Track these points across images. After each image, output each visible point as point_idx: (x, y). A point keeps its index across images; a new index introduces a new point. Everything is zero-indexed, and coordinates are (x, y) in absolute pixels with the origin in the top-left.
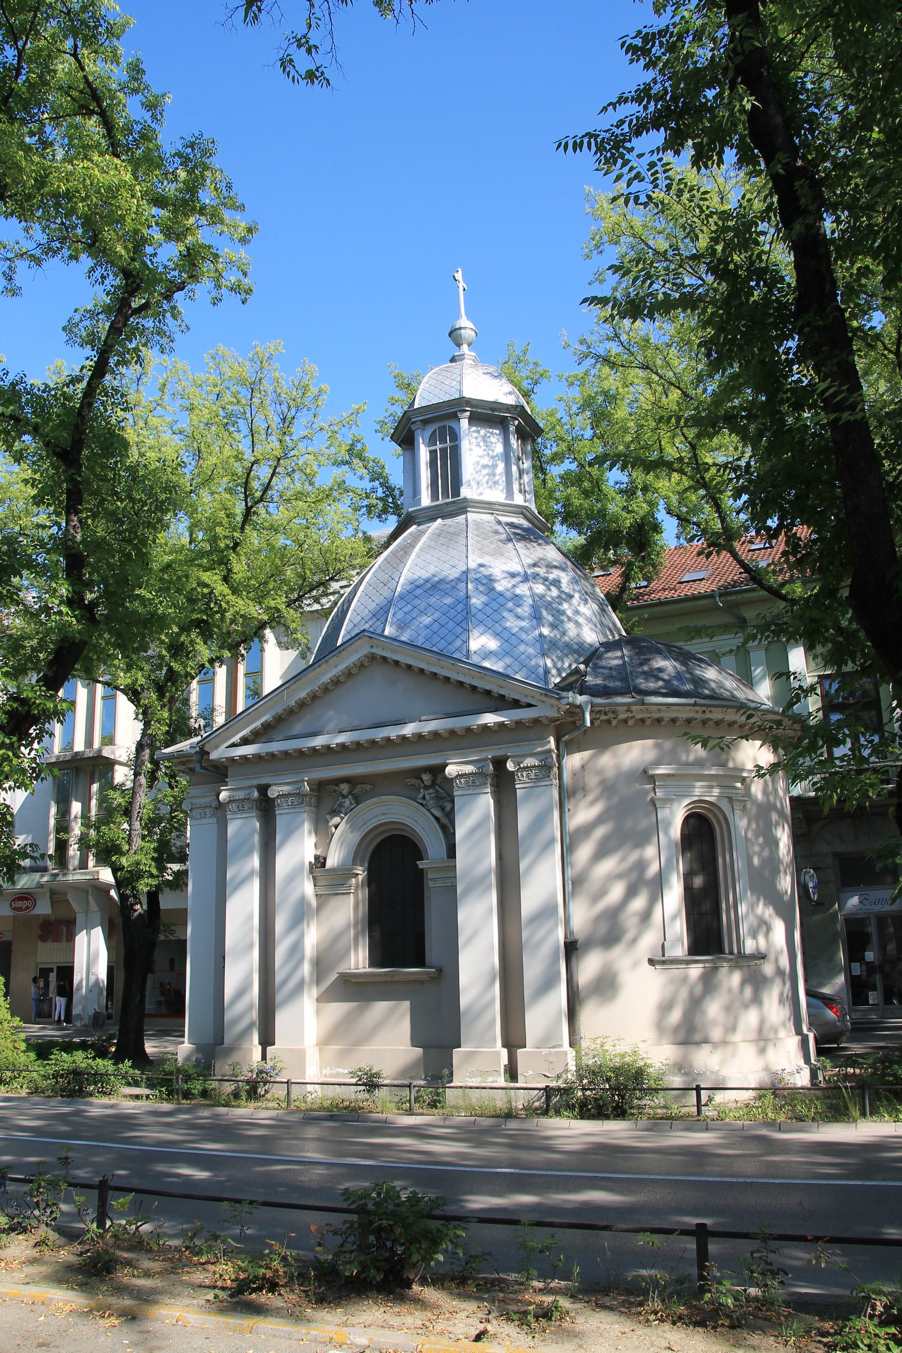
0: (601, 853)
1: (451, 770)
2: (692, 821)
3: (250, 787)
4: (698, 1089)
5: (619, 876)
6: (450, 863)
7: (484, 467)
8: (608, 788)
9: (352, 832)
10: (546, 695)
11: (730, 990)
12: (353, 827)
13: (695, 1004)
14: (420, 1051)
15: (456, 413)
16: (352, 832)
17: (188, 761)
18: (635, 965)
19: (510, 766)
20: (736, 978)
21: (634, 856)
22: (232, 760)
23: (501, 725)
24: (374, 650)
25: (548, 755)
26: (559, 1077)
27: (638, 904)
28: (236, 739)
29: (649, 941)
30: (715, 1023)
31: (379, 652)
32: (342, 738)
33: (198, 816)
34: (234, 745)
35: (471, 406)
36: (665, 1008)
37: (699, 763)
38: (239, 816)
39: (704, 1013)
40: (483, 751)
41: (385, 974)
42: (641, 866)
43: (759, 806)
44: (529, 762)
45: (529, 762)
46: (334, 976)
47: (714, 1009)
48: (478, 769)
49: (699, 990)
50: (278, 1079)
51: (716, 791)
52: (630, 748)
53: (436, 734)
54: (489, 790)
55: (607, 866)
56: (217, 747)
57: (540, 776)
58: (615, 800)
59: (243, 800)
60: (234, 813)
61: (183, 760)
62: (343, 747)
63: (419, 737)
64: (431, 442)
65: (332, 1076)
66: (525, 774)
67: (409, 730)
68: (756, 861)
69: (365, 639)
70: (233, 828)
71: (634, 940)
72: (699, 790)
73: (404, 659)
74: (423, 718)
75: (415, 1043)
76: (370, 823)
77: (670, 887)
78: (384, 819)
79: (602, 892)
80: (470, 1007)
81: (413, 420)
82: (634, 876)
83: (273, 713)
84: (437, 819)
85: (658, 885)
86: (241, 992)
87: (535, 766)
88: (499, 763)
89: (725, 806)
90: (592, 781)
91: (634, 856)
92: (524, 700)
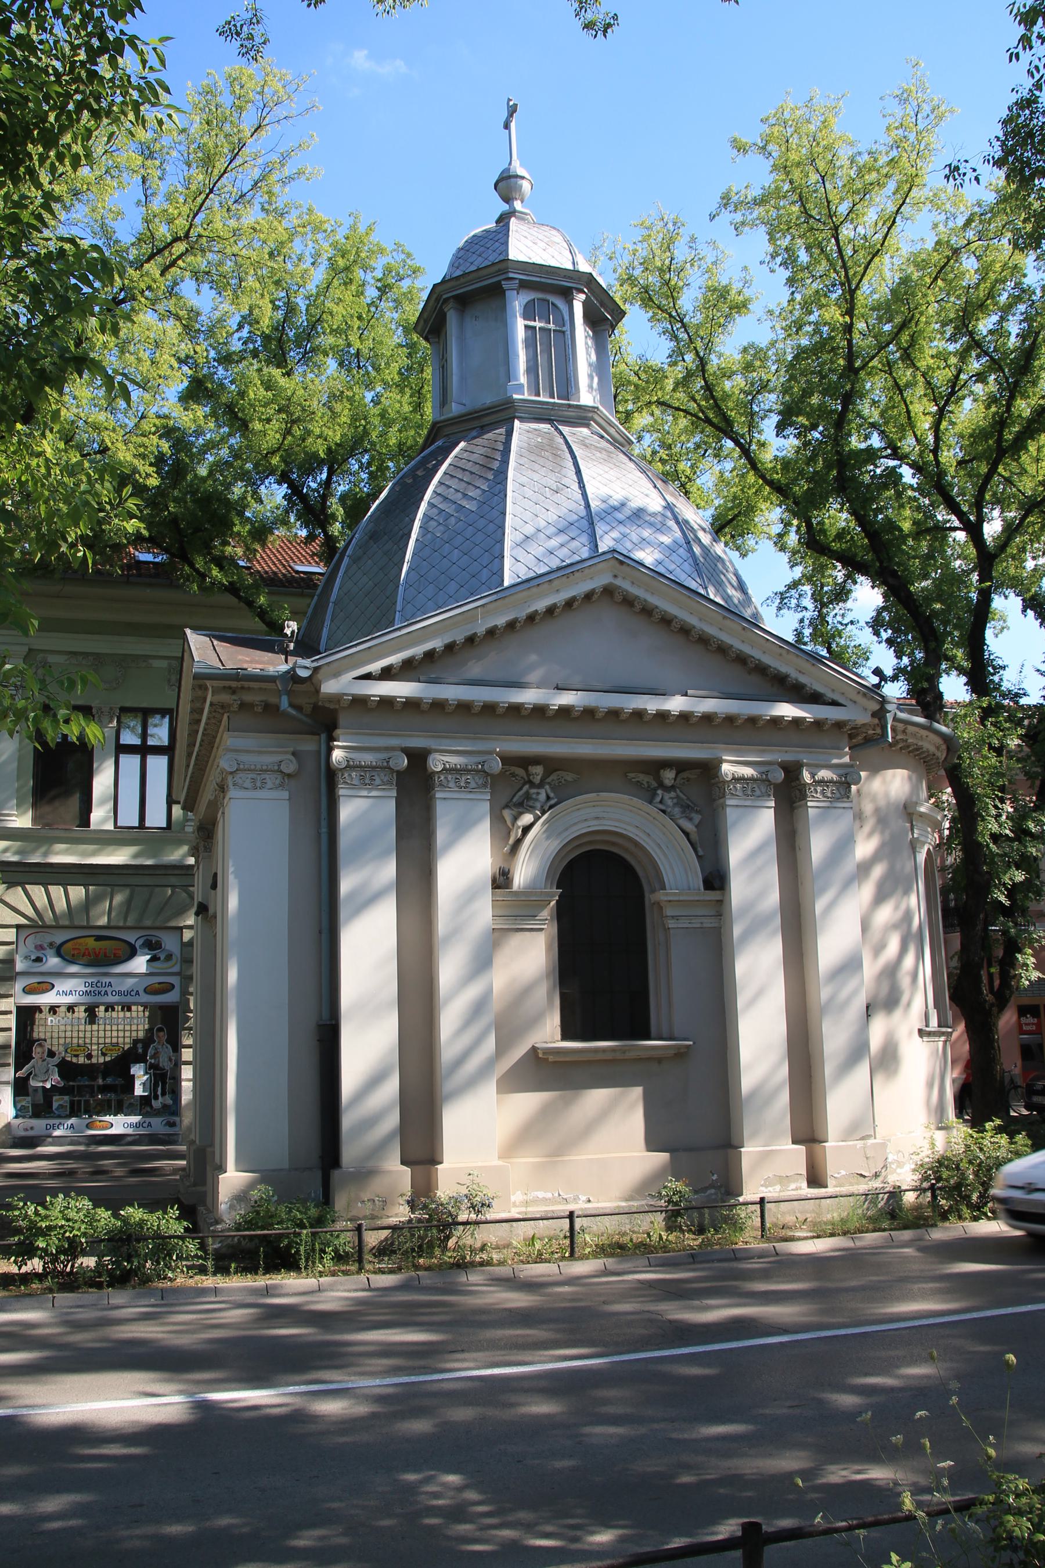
3: (392, 749)
5: (895, 926)
10: (865, 695)
12: (549, 832)
14: (664, 1156)
15: (571, 288)
16: (548, 838)
19: (807, 777)
22: (360, 702)
23: (797, 722)
24: (618, 582)
26: (876, 1175)
28: (375, 667)
31: (626, 585)
32: (567, 699)
33: (248, 784)
34: (368, 677)
38: (365, 793)
40: (764, 751)
44: (824, 774)
45: (824, 774)
48: (761, 773)
50: (490, 1216)
53: (708, 718)
54: (772, 804)
56: (337, 674)
57: (838, 795)
59: (373, 768)
60: (353, 787)
61: (234, 684)
62: (565, 711)
63: (685, 717)
65: (527, 1203)
66: (819, 789)
67: (676, 704)
69: (613, 562)
70: (349, 810)
71: (909, 1004)
74: (690, 692)
75: (653, 1143)
78: (595, 826)
81: (511, 275)
83: (448, 640)
84: (687, 834)
86: (374, 1081)
88: (792, 771)
92: (830, 695)
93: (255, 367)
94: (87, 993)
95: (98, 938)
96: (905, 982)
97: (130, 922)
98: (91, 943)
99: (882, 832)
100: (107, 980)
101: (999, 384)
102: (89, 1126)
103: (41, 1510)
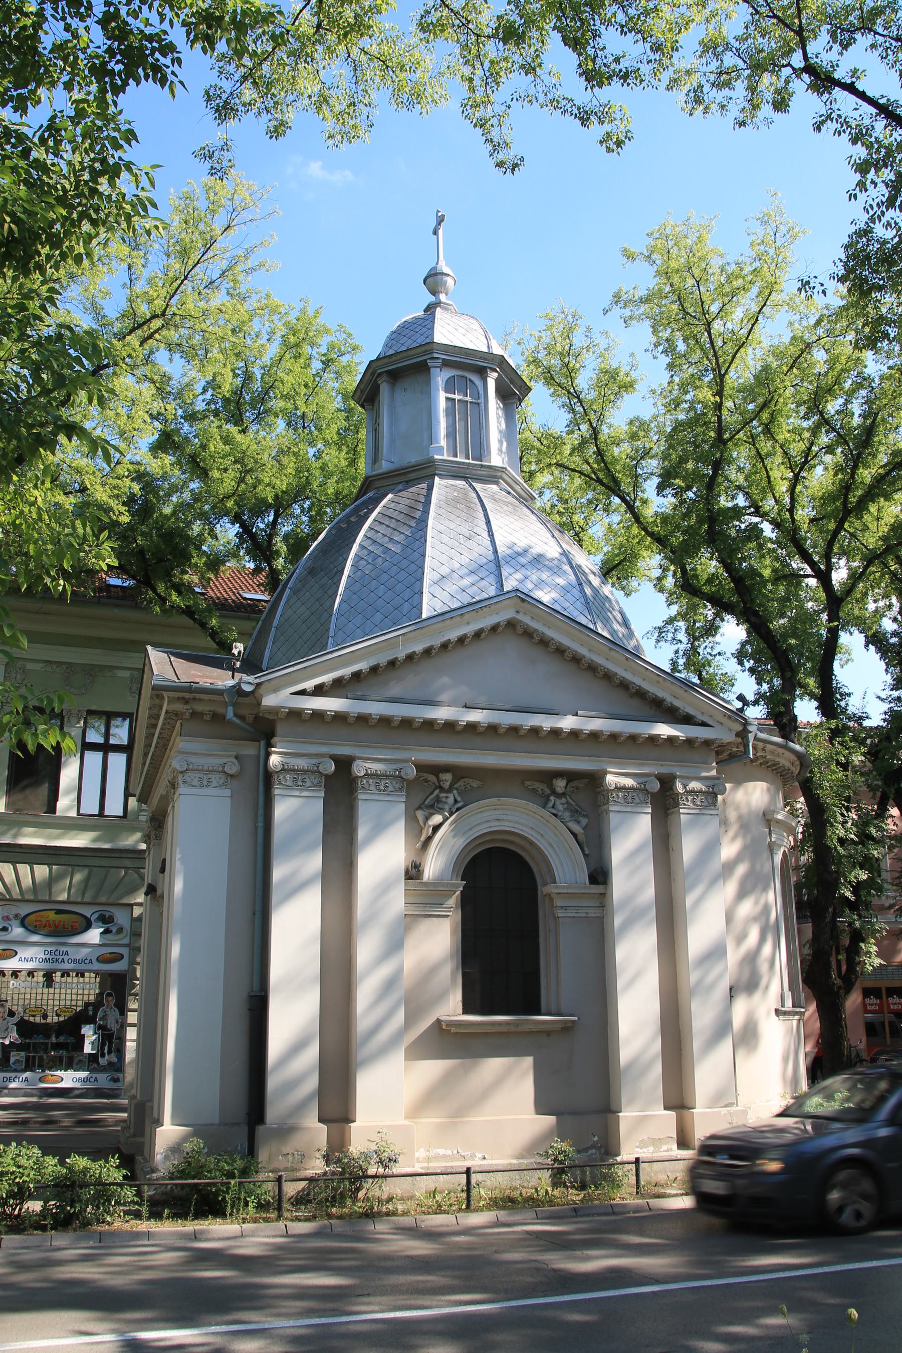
1: (611, 780)
3: (322, 755)
6: (597, 889)
9: (454, 836)
10: (730, 717)
12: (456, 830)
15: (486, 368)
16: (454, 836)
17: (194, 699)
23: (671, 740)
24: (520, 617)
25: (717, 782)
28: (309, 685)
31: (526, 620)
32: (475, 716)
34: (303, 693)
38: (297, 793)
40: (643, 764)
41: (507, 1023)
44: (694, 785)
46: (426, 1023)
48: (708, 787)
53: (595, 735)
56: (276, 690)
57: (706, 804)
59: (305, 772)
61: (187, 695)
63: (575, 734)
64: (450, 387)
65: (429, 1159)
66: (690, 798)
67: (568, 723)
73: (469, 629)
75: (541, 1108)
76: (476, 829)
80: (631, 1064)
81: (435, 355)
84: (575, 835)
87: (700, 792)
88: (667, 782)
92: (700, 717)
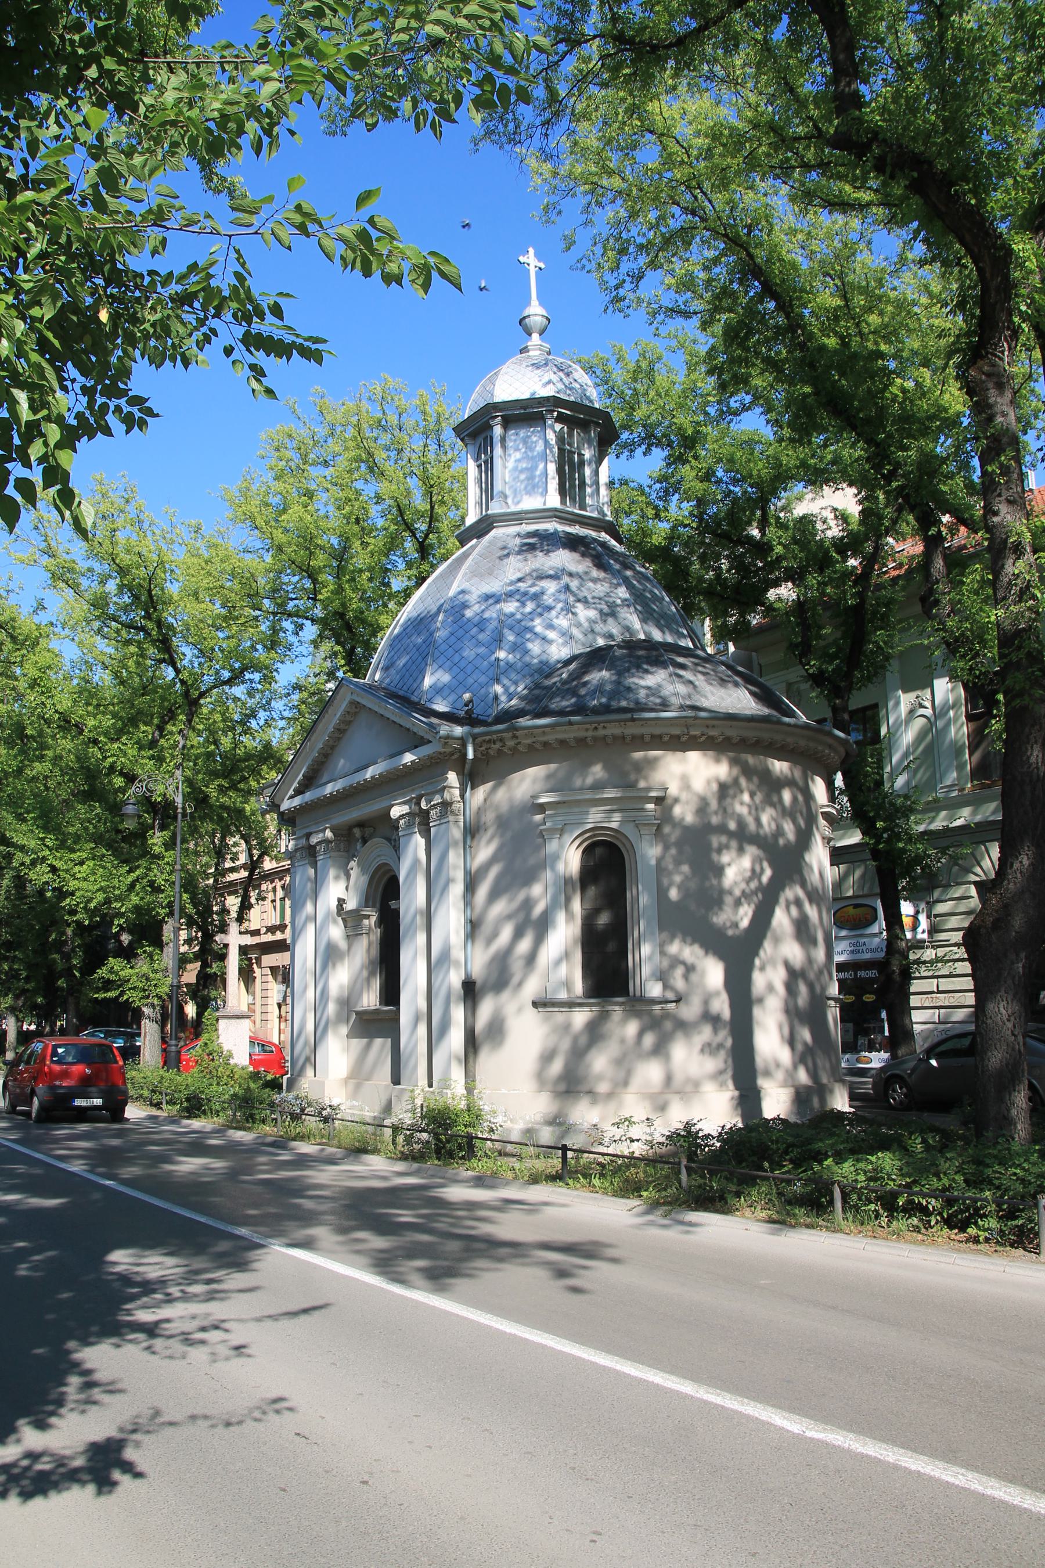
0: (494, 895)
1: (396, 812)
2: (599, 851)
4: (565, 1149)
5: (509, 917)
7: (521, 471)
8: (503, 823)
11: (623, 1041)
13: (579, 1053)
18: (520, 1010)
20: (632, 1028)
21: (521, 896)
27: (524, 945)
29: (532, 987)
30: (600, 1078)
35: (500, 410)
36: (547, 1057)
37: (598, 786)
39: (589, 1066)
42: (528, 904)
43: (687, 830)
47: (600, 1062)
49: (583, 1041)
51: (617, 817)
52: (522, 780)
55: (499, 908)
58: (509, 834)
68: (674, 894)
71: (520, 984)
72: (594, 817)
77: (554, 927)
79: (495, 935)
82: (521, 916)
85: (542, 927)
89: (629, 831)
90: (489, 817)
91: (521, 896)
93: (696, 418)
94: (852, 952)
95: (856, 906)
96: (517, 966)
97: (866, 891)
98: (851, 911)
99: (502, 836)
100: (862, 940)
101: (1029, 120)
102: (858, 1061)
103: (170, 1261)
